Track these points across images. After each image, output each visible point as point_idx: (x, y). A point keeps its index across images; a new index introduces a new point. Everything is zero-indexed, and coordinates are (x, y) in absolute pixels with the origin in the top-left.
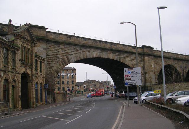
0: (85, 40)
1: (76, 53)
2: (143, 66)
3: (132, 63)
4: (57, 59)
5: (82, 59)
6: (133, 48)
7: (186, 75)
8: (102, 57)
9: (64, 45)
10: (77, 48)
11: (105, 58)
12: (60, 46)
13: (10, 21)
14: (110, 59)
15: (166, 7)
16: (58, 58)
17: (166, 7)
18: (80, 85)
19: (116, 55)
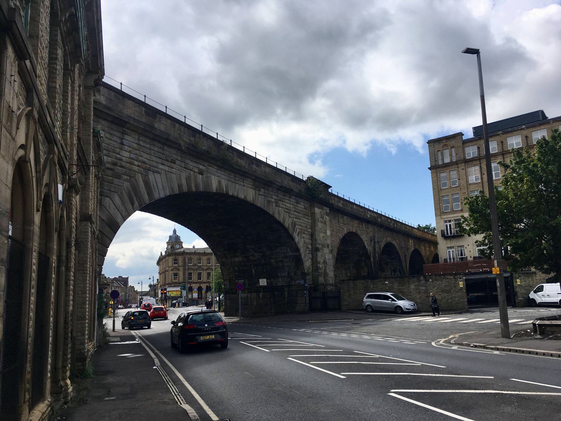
0: (194, 136)
1: (170, 170)
2: (310, 230)
3: (291, 220)
4: (116, 181)
5: (184, 191)
6: (292, 181)
7: (53, 301)
8: (231, 193)
9: (137, 137)
10: (172, 153)
11: (237, 198)
12: (126, 137)
13: (123, 317)
14: (247, 201)
15: (161, 252)
16: (119, 177)
17: (161, 252)
18: (451, 188)
19: (261, 193)
